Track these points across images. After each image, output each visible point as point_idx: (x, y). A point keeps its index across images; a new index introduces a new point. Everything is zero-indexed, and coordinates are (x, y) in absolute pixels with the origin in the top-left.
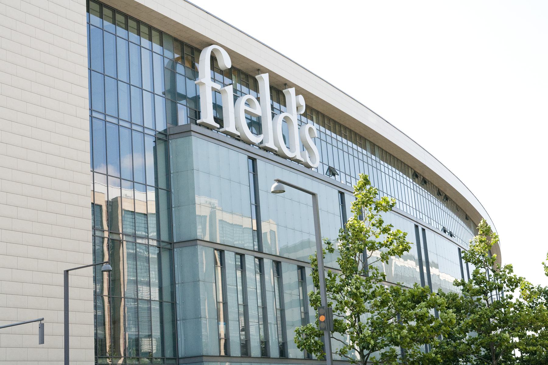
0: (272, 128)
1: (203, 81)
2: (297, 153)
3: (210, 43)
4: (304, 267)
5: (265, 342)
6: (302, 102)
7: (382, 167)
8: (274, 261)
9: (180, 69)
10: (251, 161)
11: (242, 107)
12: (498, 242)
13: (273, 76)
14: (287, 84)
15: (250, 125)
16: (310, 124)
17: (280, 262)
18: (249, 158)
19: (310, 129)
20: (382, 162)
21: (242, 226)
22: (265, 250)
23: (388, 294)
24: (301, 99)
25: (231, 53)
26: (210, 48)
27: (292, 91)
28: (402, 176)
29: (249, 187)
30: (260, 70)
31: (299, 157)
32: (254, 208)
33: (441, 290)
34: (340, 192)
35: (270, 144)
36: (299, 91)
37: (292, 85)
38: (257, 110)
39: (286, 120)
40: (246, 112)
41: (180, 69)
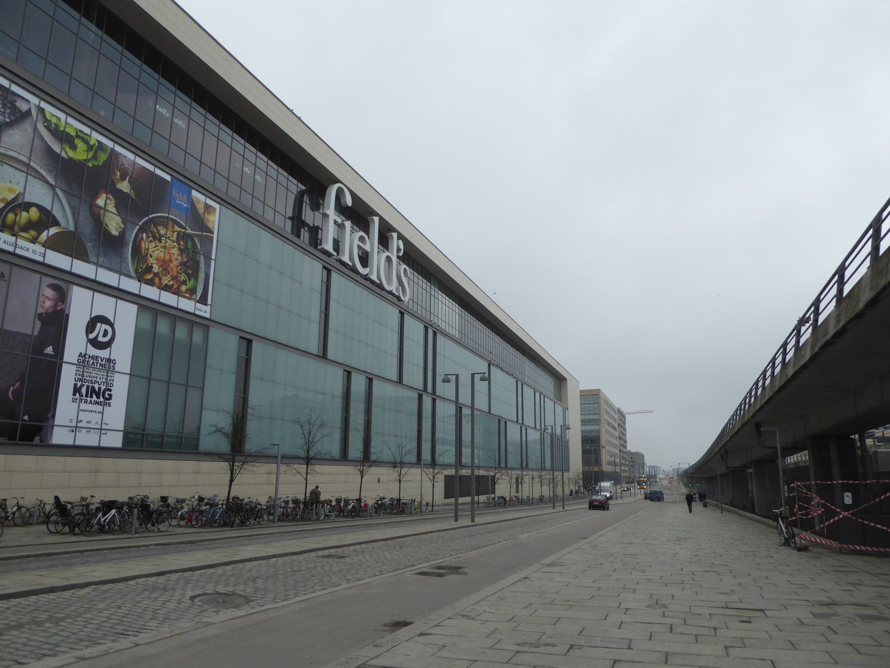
0: (349, 244)
1: (328, 212)
2: (393, 287)
3: (338, 181)
4: (372, 379)
5: (161, 445)
6: (402, 246)
7: (440, 297)
8: (367, 377)
9: (306, 199)
10: (325, 272)
11: (357, 242)
12: (320, 231)
13: (382, 221)
14: (391, 229)
15: (360, 258)
16: (404, 266)
17: (372, 379)
18: (324, 267)
19: (405, 270)
20: (440, 292)
21: (561, 426)
22: (437, 393)
23: (215, 334)
24: (401, 243)
25: (354, 196)
26: (336, 186)
27: (395, 235)
28: (287, 177)
29: (320, 295)
30: (373, 213)
31: (394, 291)
32: (323, 315)
33: (569, 429)
34: (425, 326)
35: (374, 277)
36: (401, 237)
37: (395, 231)
38: (367, 248)
39: (389, 259)
40: (359, 247)
41: (306, 199)
